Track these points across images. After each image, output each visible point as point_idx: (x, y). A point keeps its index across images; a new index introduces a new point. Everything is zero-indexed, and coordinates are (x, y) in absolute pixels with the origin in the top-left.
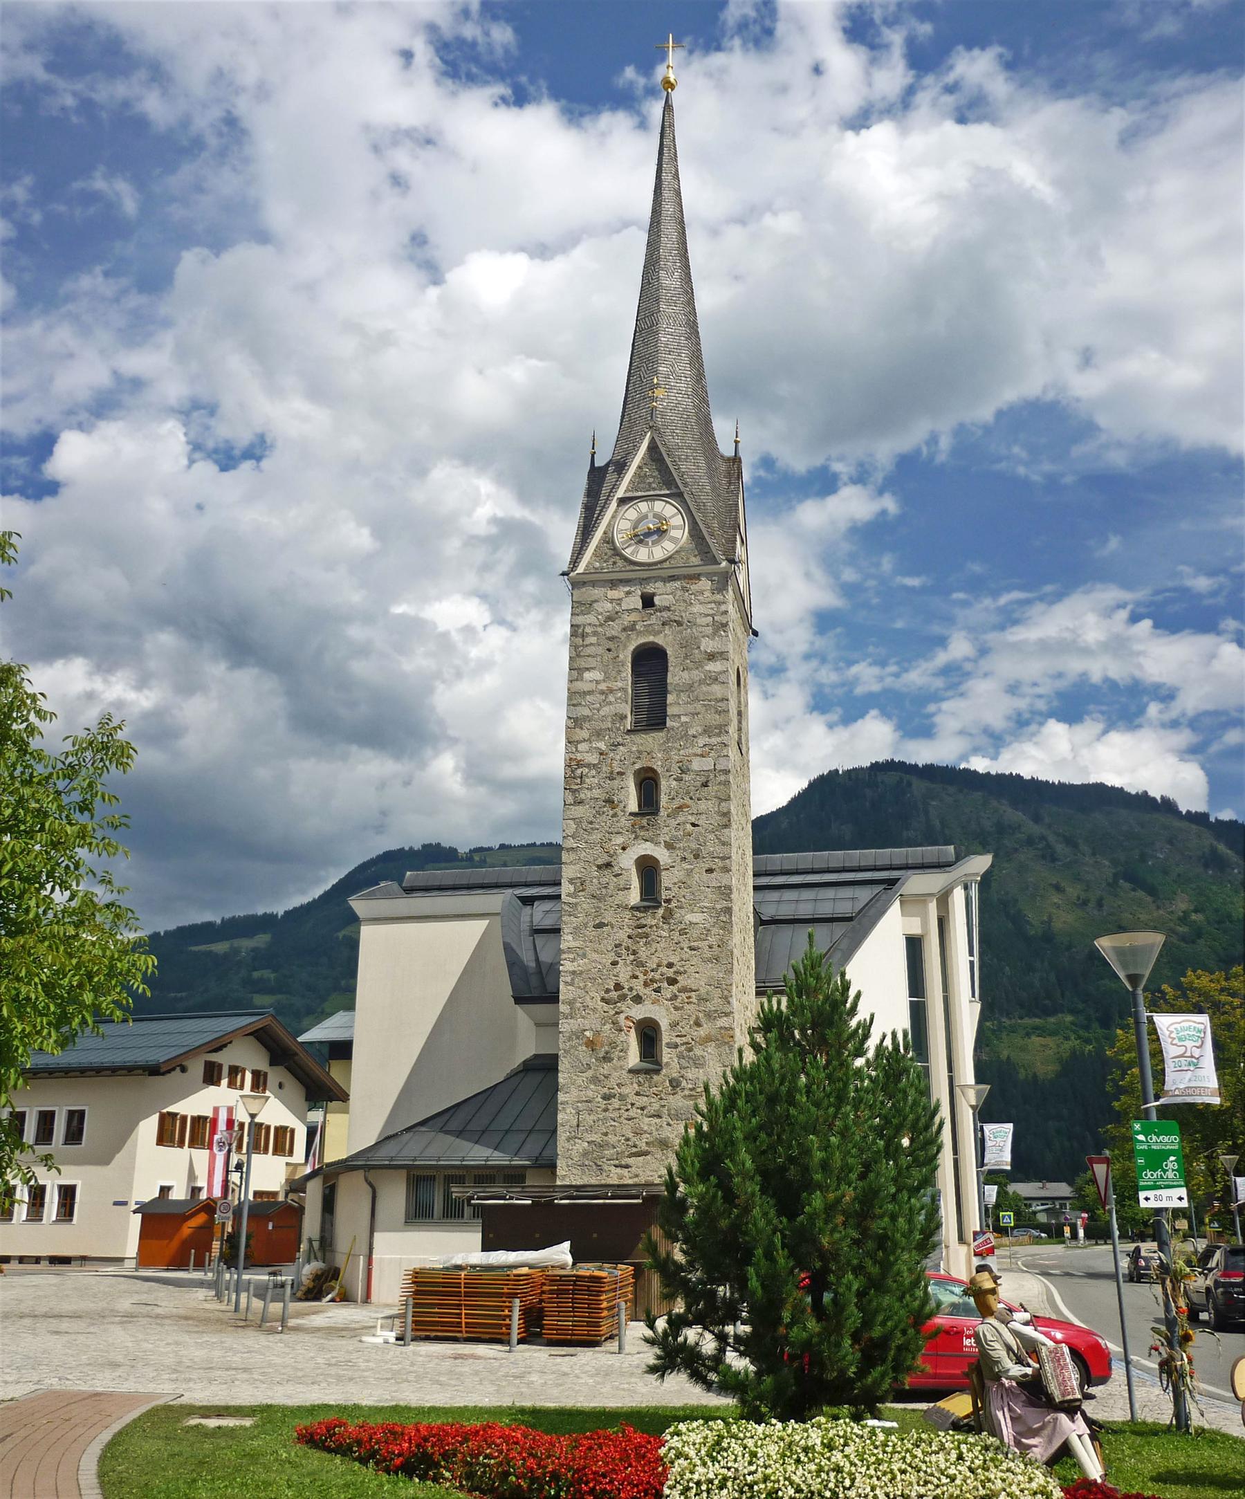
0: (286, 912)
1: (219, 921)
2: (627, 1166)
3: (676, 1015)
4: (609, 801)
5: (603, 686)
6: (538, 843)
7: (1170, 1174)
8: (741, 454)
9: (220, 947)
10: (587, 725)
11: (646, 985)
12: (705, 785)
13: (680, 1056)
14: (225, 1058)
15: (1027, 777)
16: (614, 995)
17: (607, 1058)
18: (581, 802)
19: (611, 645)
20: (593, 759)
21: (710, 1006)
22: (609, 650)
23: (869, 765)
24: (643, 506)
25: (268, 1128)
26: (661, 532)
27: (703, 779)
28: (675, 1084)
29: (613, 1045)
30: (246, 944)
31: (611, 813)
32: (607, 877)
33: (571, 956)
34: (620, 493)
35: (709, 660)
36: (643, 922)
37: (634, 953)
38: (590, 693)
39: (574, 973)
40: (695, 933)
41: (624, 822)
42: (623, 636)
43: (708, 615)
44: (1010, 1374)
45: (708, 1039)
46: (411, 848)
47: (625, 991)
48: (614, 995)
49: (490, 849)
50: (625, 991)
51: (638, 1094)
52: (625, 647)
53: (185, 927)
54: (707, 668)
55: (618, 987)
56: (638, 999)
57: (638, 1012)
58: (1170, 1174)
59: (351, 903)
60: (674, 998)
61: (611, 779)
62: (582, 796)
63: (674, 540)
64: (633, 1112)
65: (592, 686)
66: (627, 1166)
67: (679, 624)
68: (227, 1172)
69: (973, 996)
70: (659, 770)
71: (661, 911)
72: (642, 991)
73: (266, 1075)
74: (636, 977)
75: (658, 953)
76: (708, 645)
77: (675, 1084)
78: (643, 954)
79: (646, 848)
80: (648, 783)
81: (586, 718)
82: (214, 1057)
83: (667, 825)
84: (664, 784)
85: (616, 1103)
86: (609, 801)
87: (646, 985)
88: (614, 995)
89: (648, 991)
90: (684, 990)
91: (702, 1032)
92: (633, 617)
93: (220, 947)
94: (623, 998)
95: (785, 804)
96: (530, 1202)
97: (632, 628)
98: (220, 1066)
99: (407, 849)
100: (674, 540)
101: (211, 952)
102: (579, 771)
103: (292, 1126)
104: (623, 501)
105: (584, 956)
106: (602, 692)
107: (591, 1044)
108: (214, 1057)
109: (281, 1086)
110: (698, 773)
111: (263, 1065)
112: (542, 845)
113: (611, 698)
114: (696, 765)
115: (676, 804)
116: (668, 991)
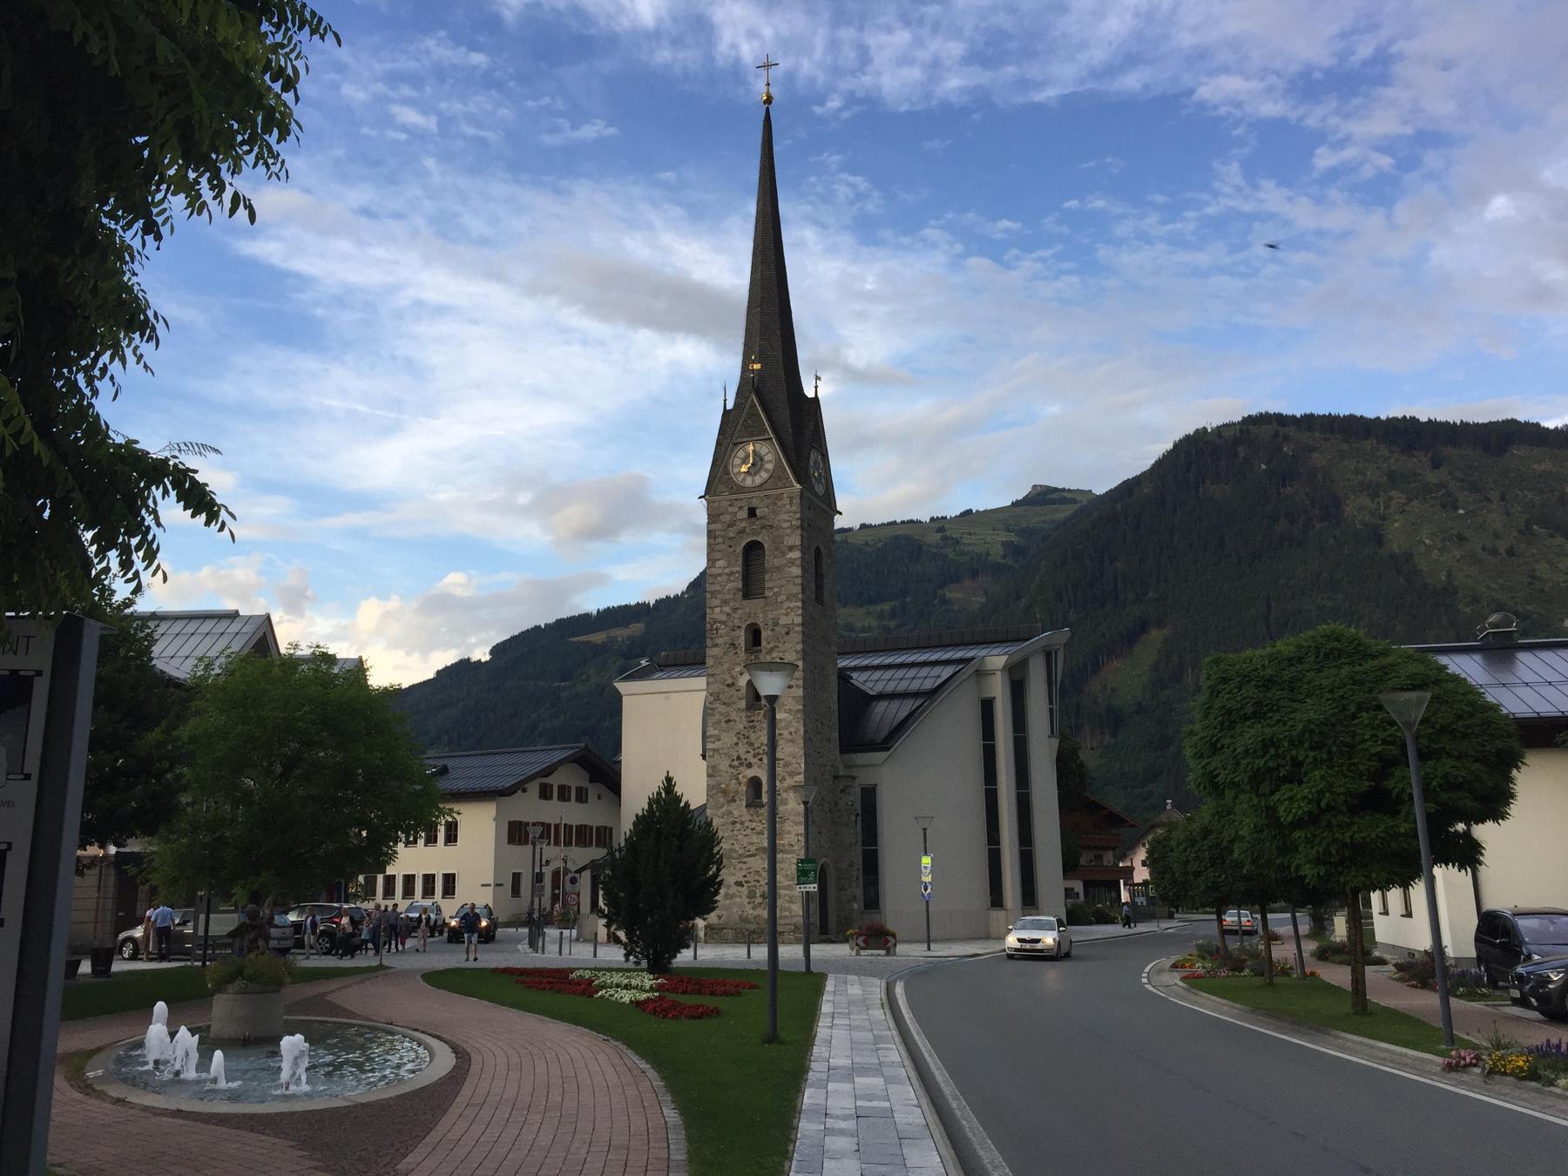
1: (595, 613)
2: (744, 863)
4: (733, 644)
5: (727, 571)
6: (899, 521)
7: (811, 879)
8: (819, 396)
9: (598, 638)
10: (720, 596)
11: (755, 756)
12: (787, 633)
14: (555, 780)
15: (1424, 419)
16: (736, 763)
18: (716, 645)
19: (730, 543)
20: (724, 618)
21: (790, 769)
22: (730, 546)
23: (1240, 419)
25: (591, 828)
27: (786, 630)
30: (621, 633)
31: (734, 652)
33: (712, 740)
35: (790, 551)
36: (752, 718)
37: (748, 738)
38: (720, 575)
39: (713, 750)
43: (788, 521)
47: (743, 760)
49: (850, 530)
50: (743, 760)
51: (750, 821)
52: (740, 544)
53: (563, 619)
54: (788, 556)
55: (739, 758)
56: (749, 765)
58: (811, 879)
59: (615, 684)
61: (733, 630)
62: (718, 642)
64: (748, 832)
65: (720, 571)
66: (744, 863)
67: (771, 527)
68: (541, 866)
69: (1052, 733)
70: (761, 625)
72: (754, 761)
73: (587, 790)
74: (749, 752)
78: (753, 737)
80: (755, 636)
81: (718, 592)
82: (545, 780)
84: (763, 633)
85: (738, 826)
87: (755, 756)
89: (756, 760)
92: (744, 524)
93: (598, 638)
94: (742, 764)
95: (1100, 490)
97: (742, 532)
98: (552, 786)
101: (590, 642)
102: (715, 626)
103: (609, 825)
105: (719, 740)
106: (727, 574)
108: (545, 780)
109: (599, 797)
110: (784, 626)
111: (584, 783)
112: (903, 522)
113: (732, 578)
114: (784, 621)
115: (772, 645)
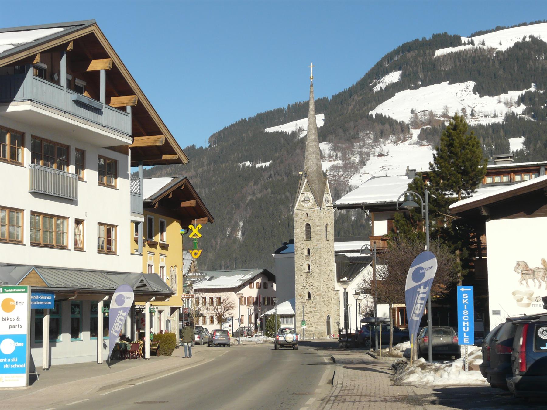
0: (333, 97)
1: (286, 107)
3: (313, 291)
13: (313, 298)
17: (302, 298)
24: (306, 195)
26: (309, 201)
28: (313, 302)
29: (303, 296)
32: (302, 267)
34: (301, 192)
40: (315, 277)
41: (304, 258)
42: (303, 222)
44: (159, 317)
45: (317, 295)
46: (424, 39)
48: (303, 288)
55: (304, 286)
57: (308, 290)
60: (312, 288)
63: (311, 203)
67: (312, 220)
71: (310, 273)
72: (308, 287)
73: (267, 284)
75: (310, 280)
76: (317, 224)
77: (313, 302)
78: (308, 280)
79: (308, 262)
83: (311, 258)
86: (302, 254)
88: (303, 288)
90: (314, 287)
91: (317, 294)
96: (400, 313)
99: (420, 39)
100: (311, 203)
104: (302, 194)
107: (300, 296)
116: (312, 287)
